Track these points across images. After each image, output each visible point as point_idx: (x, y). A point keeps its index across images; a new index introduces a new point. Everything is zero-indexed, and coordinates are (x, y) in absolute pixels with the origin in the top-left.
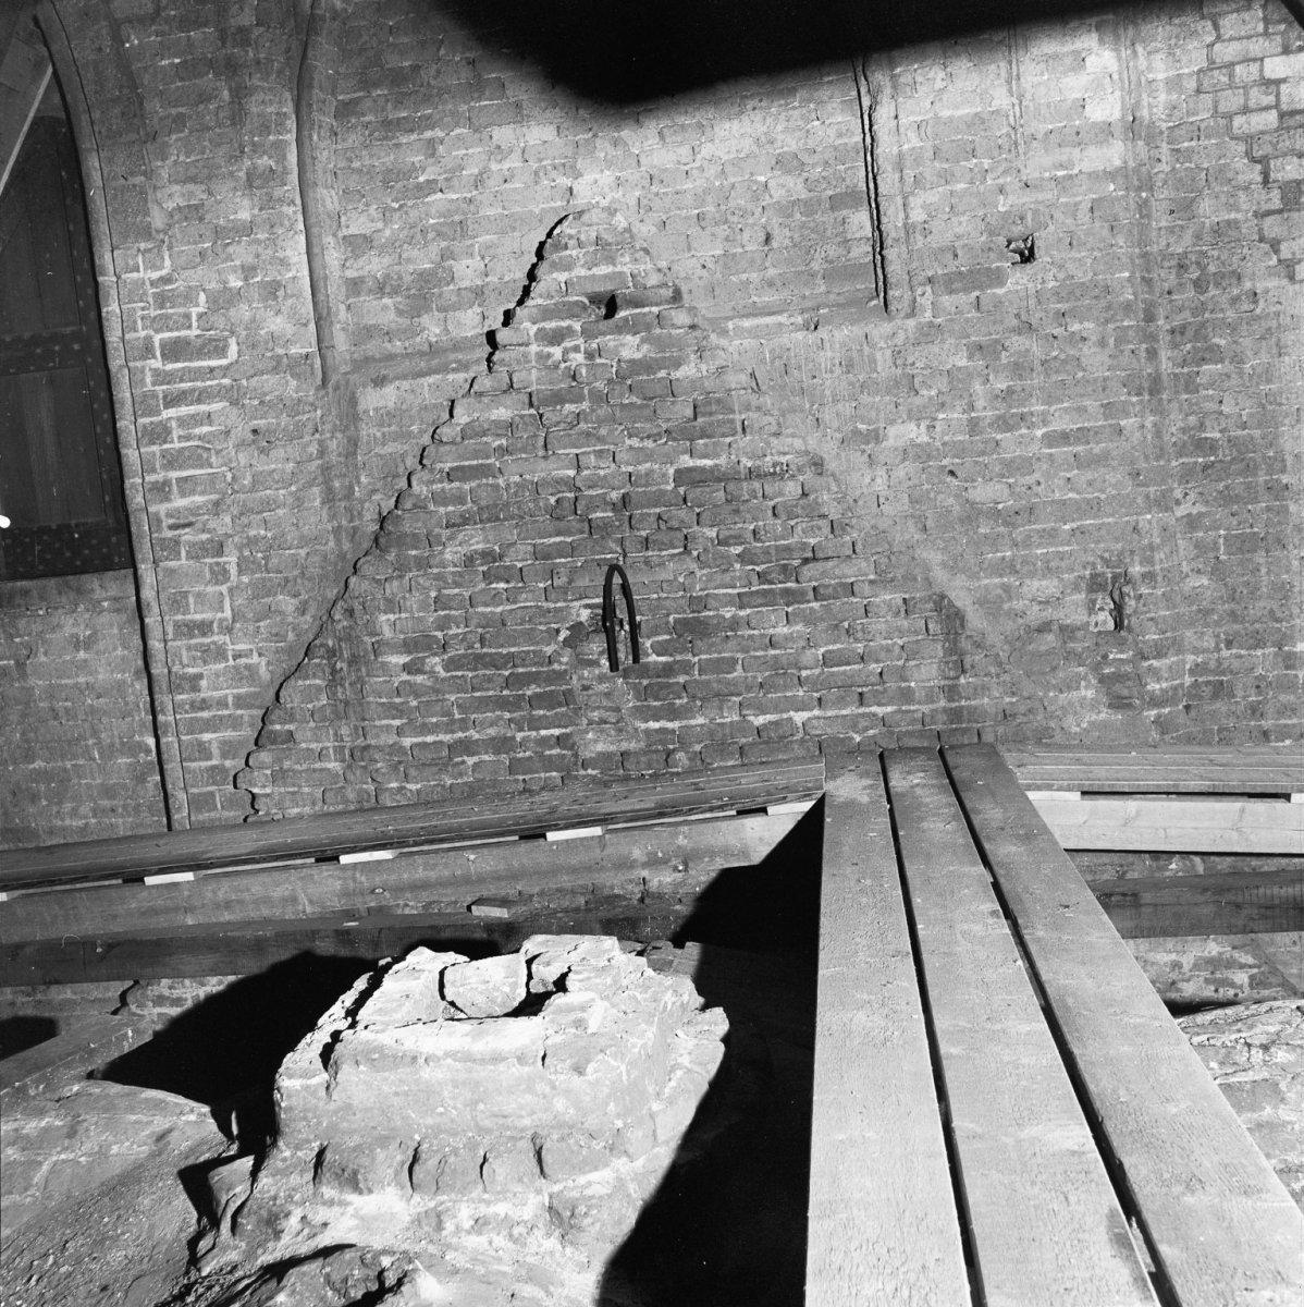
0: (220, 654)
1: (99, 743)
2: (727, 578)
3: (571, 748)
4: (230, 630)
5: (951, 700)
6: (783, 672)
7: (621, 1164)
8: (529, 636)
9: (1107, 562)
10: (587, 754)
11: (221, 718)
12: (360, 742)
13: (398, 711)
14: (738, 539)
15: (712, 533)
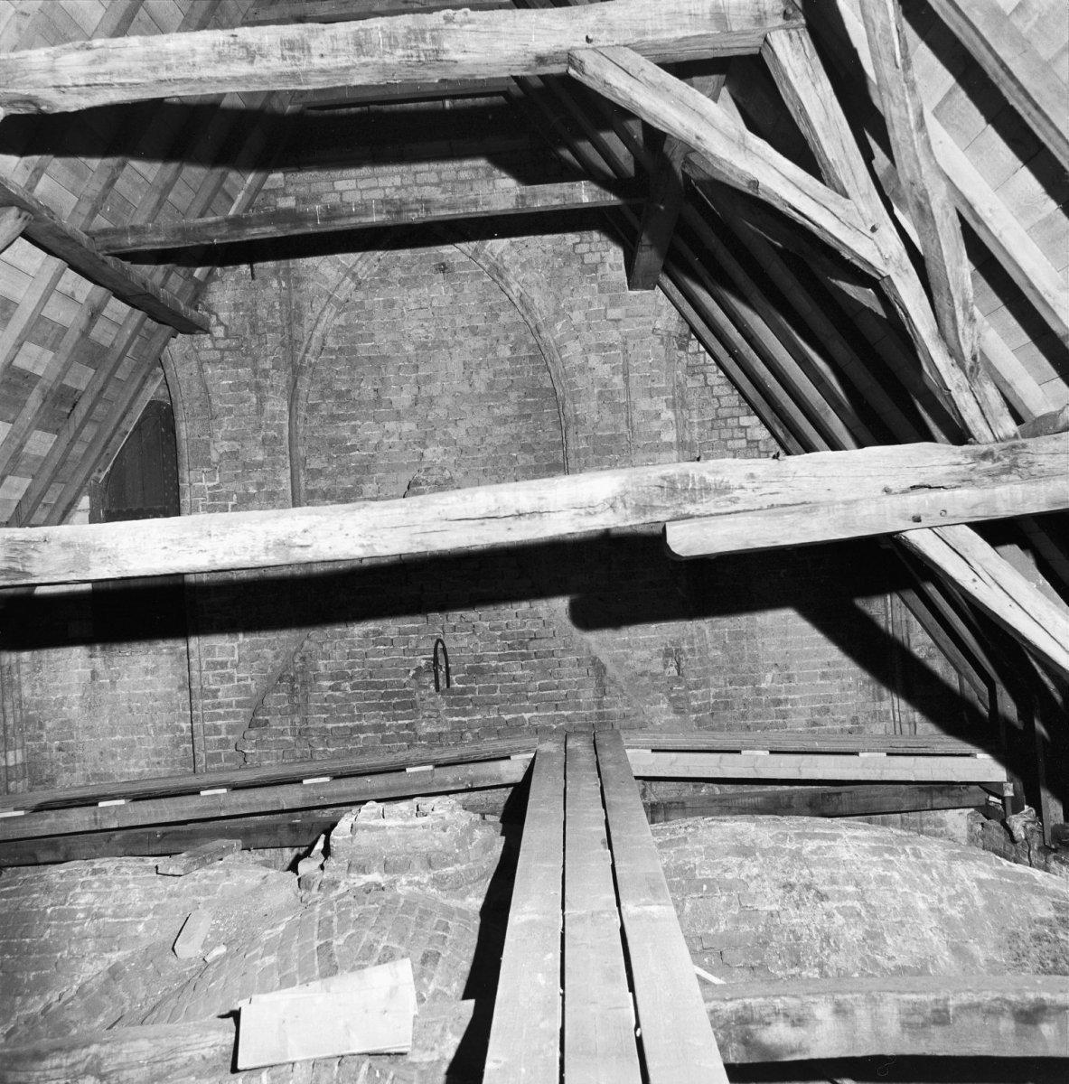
0: (231, 679)
1: (154, 725)
2: (493, 647)
3: (414, 730)
4: (236, 666)
5: (599, 708)
6: (519, 694)
7: (458, 866)
8: (396, 673)
9: (672, 643)
10: (421, 733)
11: (228, 713)
12: (305, 726)
13: (325, 710)
14: (499, 628)
15: (487, 624)
